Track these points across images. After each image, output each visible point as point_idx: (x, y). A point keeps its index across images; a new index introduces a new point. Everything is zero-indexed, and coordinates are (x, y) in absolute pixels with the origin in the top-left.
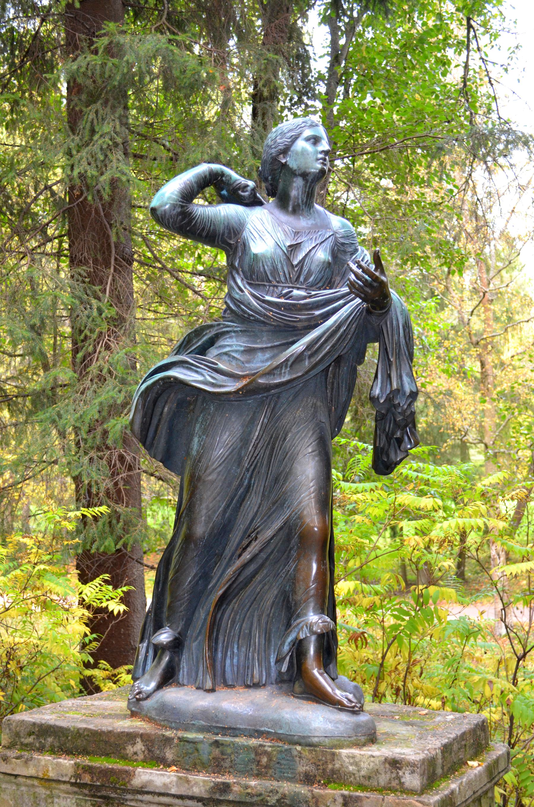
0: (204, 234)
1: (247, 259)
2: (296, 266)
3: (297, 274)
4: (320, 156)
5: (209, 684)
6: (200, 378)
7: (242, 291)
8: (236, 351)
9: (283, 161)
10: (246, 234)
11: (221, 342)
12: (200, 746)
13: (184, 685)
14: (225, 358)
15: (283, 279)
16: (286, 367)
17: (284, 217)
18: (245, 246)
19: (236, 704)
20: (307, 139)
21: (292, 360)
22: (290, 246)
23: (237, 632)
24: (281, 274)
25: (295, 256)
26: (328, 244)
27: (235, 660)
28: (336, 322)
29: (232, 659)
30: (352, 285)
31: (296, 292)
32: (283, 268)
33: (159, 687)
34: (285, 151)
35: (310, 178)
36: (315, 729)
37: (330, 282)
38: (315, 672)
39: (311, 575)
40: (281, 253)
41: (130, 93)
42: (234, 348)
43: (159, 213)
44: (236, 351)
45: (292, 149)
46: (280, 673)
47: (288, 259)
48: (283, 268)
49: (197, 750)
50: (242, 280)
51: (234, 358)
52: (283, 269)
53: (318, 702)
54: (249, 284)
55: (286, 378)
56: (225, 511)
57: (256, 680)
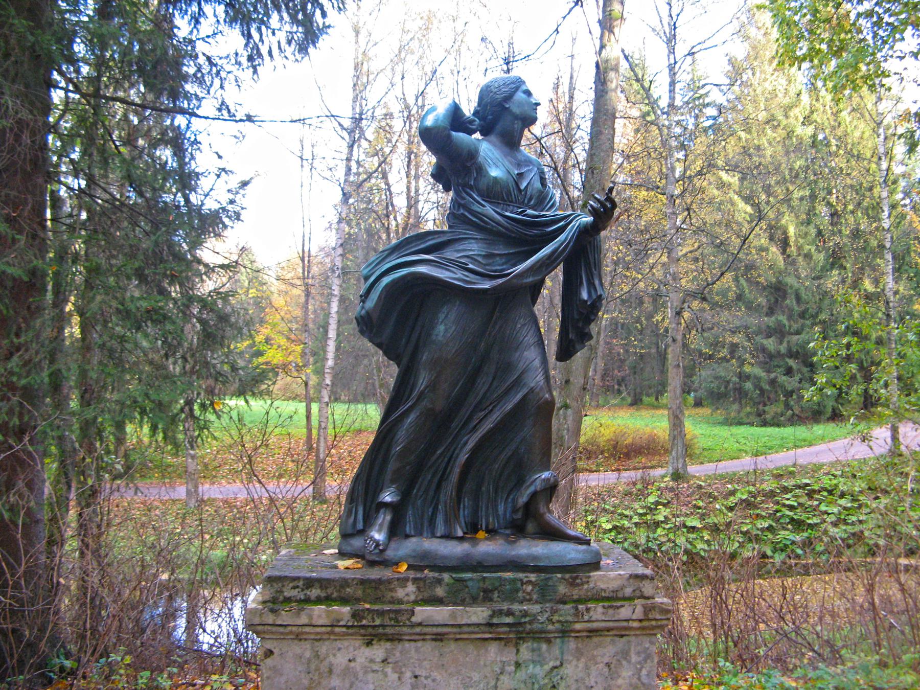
12: (470, 584)
18: (480, 170)
19: (488, 547)
31: (530, 212)
34: (509, 97)
49: (467, 587)
51: (476, 260)
53: (552, 540)
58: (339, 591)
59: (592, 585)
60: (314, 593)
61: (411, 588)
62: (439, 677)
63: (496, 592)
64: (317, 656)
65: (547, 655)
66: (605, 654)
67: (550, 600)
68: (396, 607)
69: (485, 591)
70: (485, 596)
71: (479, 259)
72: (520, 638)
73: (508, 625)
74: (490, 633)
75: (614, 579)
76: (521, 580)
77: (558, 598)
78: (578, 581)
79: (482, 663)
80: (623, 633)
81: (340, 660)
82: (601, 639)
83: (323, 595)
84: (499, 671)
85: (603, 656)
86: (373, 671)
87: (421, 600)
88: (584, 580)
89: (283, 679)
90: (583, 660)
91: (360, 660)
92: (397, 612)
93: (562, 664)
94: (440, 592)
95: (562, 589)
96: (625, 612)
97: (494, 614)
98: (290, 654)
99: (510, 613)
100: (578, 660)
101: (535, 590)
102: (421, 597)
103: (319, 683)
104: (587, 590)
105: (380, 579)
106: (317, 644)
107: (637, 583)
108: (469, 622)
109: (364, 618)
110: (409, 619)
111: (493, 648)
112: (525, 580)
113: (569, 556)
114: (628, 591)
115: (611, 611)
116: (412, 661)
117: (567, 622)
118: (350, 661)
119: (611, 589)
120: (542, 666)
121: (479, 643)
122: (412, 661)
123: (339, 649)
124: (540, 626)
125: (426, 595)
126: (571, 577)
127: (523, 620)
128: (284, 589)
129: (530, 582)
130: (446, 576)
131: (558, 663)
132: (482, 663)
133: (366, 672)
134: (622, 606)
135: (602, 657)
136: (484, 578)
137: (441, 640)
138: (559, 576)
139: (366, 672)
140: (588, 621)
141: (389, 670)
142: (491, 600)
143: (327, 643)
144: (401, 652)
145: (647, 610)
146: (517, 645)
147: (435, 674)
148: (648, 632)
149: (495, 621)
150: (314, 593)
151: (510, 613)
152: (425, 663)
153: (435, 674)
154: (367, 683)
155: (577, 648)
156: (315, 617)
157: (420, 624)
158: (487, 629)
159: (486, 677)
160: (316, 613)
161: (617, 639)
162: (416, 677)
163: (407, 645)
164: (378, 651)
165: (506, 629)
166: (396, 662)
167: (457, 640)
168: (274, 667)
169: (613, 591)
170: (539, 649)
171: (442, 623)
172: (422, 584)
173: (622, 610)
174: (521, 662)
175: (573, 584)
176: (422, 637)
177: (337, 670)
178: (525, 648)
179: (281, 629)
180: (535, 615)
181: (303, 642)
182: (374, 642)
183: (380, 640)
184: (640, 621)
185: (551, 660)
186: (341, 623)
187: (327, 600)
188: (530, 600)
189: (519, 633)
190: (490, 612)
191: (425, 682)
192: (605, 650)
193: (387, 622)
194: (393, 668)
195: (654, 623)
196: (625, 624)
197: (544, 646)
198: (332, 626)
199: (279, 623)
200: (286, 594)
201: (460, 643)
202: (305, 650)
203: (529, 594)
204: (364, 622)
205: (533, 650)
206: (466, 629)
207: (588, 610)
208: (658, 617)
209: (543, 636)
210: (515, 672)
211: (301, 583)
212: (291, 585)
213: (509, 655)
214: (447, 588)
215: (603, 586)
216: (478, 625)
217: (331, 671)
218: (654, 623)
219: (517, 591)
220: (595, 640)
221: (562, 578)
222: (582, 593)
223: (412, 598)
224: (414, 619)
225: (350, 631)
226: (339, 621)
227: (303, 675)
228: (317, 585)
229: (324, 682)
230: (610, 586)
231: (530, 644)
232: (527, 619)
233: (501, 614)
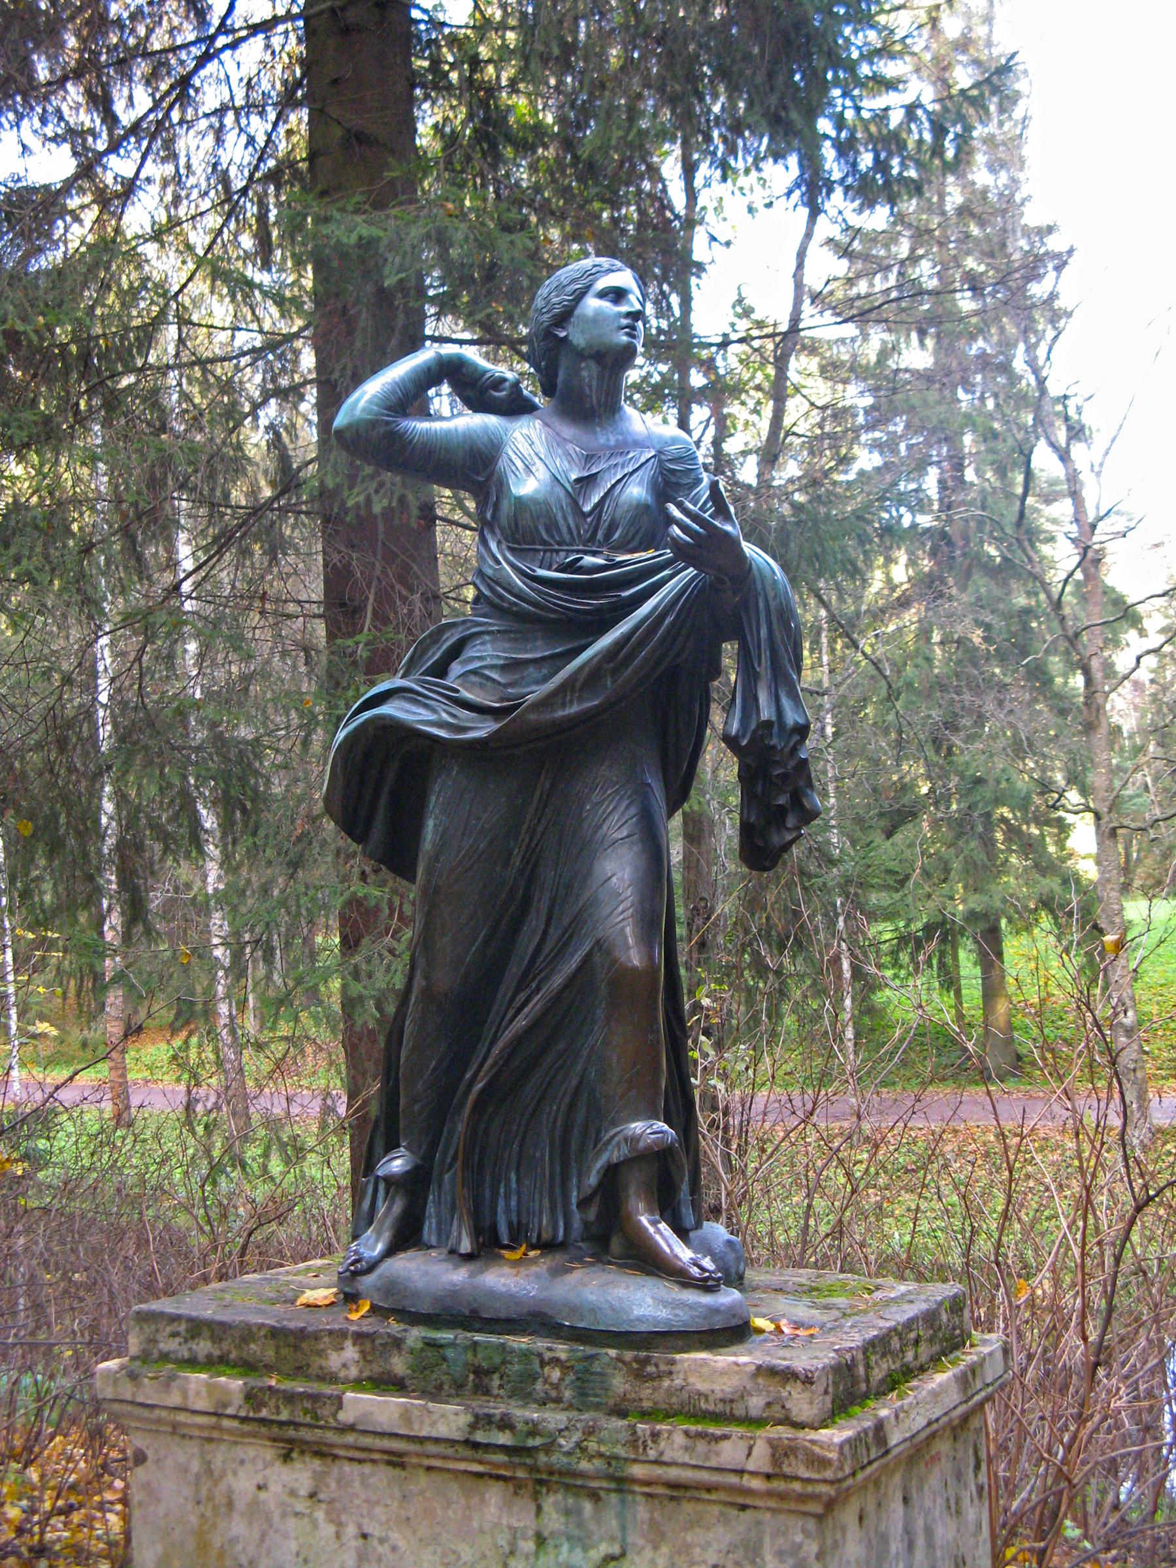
1: (505, 505)
3: (599, 529)
4: (625, 322)
5: (466, 1246)
6: (432, 717)
7: (498, 562)
8: (492, 667)
9: (563, 334)
10: (502, 463)
11: (469, 653)
12: (450, 1353)
13: (430, 1247)
14: (474, 679)
15: (567, 537)
17: (568, 431)
18: (502, 485)
19: (508, 1280)
20: (602, 295)
21: (582, 678)
22: (578, 481)
24: (564, 530)
25: (586, 498)
26: (647, 473)
27: (513, 1203)
28: (655, 608)
29: (507, 1198)
30: (676, 544)
31: (589, 560)
33: (390, 1252)
34: (565, 316)
35: (609, 360)
37: (653, 538)
38: (644, 1220)
40: (562, 494)
42: (488, 662)
43: (347, 435)
44: (492, 667)
45: (578, 312)
46: (586, 1224)
49: (445, 1359)
50: (499, 543)
51: (488, 678)
52: (566, 521)
53: (649, 1273)
54: (511, 549)
56: (487, 942)
57: (545, 1236)
58: (238, 1347)
59: (678, 1382)
60: (203, 1347)
61: (351, 1352)
62: (402, 1544)
63: (496, 1376)
64: (209, 1471)
65: (592, 1526)
66: (709, 1544)
67: (597, 1407)
68: (315, 1387)
69: (478, 1371)
70: (478, 1380)
71: (495, 675)
72: (540, 1482)
73: (504, 1448)
74: (480, 1462)
75: (723, 1373)
76: (540, 1355)
77: (611, 1402)
78: (651, 1369)
79: (475, 1524)
80: (749, 1501)
81: (243, 1484)
82: (700, 1507)
83: (217, 1353)
84: (507, 1549)
85: (705, 1546)
86: (297, 1514)
87: (370, 1379)
88: (663, 1367)
89: (161, 1510)
90: (665, 1549)
91: (275, 1488)
92: (315, 1398)
93: (623, 1554)
94: (399, 1365)
95: (619, 1383)
96: (730, 1452)
97: (481, 1421)
98: (170, 1462)
99: (505, 1424)
100: (656, 1548)
101: (568, 1380)
102: (366, 1374)
103: (215, 1526)
104: (670, 1392)
105: (302, 1330)
106: (208, 1447)
107: (775, 1389)
108: (434, 1434)
109: (264, 1405)
110: (334, 1415)
111: (494, 1494)
112: (548, 1355)
113: (638, 1312)
114: (756, 1404)
115: (701, 1446)
116: (357, 1502)
117: (616, 1458)
118: (259, 1488)
119: (720, 1395)
120: (585, 1550)
121: (469, 1483)
122: (357, 1502)
123: (242, 1462)
124: (565, 1460)
125: (376, 1368)
126: (636, 1359)
127: (531, 1442)
128: (159, 1337)
129: (556, 1361)
130: (415, 1335)
131: (616, 1549)
132: (475, 1524)
133: (284, 1515)
134: (725, 1437)
135: (704, 1549)
136: (475, 1345)
137: (402, 1466)
138: (613, 1352)
139: (284, 1515)
140: (656, 1462)
141: (320, 1515)
142: (487, 1392)
143: (223, 1447)
144: (338, 1482)
145: (780, 1452)
146: (536, 1496)
147: (395, 1536)
148: (793, 1506)
149: (480, 1437)
150: (203, 1347)
151: (505, 1424)
152: (378, 1510)
153: (395, 1536)
154: (286, 1536)
155: (652, 1520)
156: (191, 1394)
157: (352, 1428)
158: (468, 1453)
159: (484, 1557)
160: (192, 1386)
161: (733, 1512)
162: (365, 1536)
163: (347, 1468)
164: (302, 1474)
165: (501, 1458)
166: (331, 1502)
167: (429, 1469)
168: (149, 1484)
169: (723, 1401)
170: (579, 1512)
171: (388, 1429)
172: (368, 1346)
173: (725, 1445)
174: (546, 1534)
175: (639, 1374)
176: (362, 1456)
177: (240, 1504)
178: (550, 1502)
179: (146, 1413)
180: (550, 1435)
181: (187, 1442)
182: (295, 1455)
183: (302, 1452)
184: (768, 1477)
185: (601, 1539)
186: (229, 1411)
187: (212, 1364)
188: (558, 1400)
189: (529, 1470)
190: (469, 1418)
191: (380, 1549)
192: (710, 1535)
193: (300, 1418)
194: (327, 1513)
195: (797, 1486)
196: (733, 1479)
197: (588, 1507)
198: (215, 1414)
199: (140, 1399)
200: (161, 1346)
201: (435, 1476)
202: (187, 1455)
203: (556, 1386)
204: (264, 1413)
205: (567, 1512)
206: (431, 1448)
207: (655, 1436)
208: (804, 1473)
209: (579, 1482)
210: (537, 1554)
211: (182, 1328)
212: (169, 1329)
213: (522, 1518)
214: (410, 1358)
215: (701, 1386)
216: (452, 1442)
217: (230, 1504)
218: (797, 1486)
219: (534, 1378)
220: (688, 1507)
221: (619, 1359)
222: (660, 1396)
223: (354, 1372)
224: (342, 1416)
225: (247, 1428)
226: (225, 1406)
227: (190, 1506)
228: (206, 1333)
229: (222, 1525)
230: (717, 1388)
231: (559, 1497)
232: (537, 1442)
233: (490, 1423)
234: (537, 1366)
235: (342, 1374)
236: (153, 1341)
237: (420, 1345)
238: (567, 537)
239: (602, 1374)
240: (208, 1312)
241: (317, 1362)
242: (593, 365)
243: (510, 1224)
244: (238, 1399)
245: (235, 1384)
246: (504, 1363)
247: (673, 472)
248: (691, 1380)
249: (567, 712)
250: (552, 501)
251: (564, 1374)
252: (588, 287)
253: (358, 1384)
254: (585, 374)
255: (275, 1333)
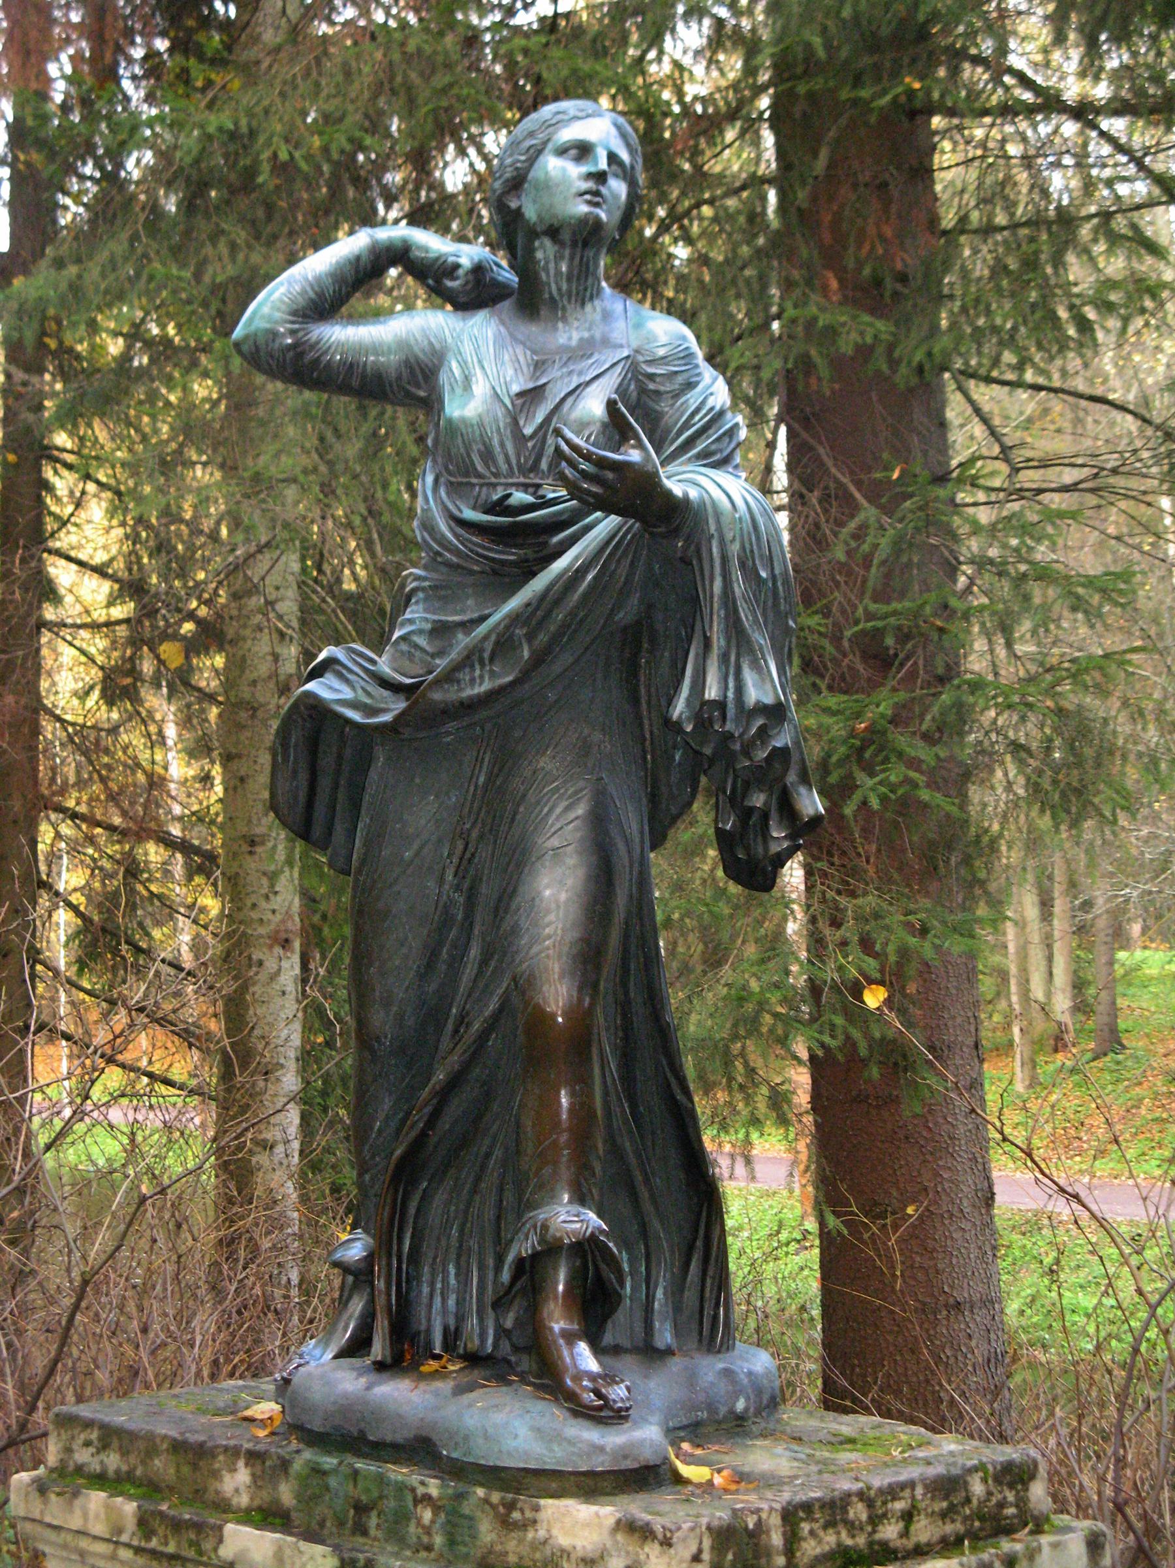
0: (355, 383)
2: (532, 437)
10: (443, 378)
12: (333, 1482)
15: (504, 467)
16: (482, 664)
19: (404, 1398)
20: (562, 152)
21: (489, 646)
22: (520, 395)
23: (454, 1242)
24: (501, 459)
27: (451, 1302)
32: (502, 445)
36: (509, 1454)
39: (558, 1113)
40: (500, 412)
41: (1103, 37)
47: (515, 422)
48: (502, 445)
52: (505, 449)
55: (486, 686)
58: (143, 1462)
59: (542, 1533)
63: (374, 1513)
78: (516, 1515)
83: (124, 1468)
102: (257, 1503)
105: (202, 1445)
110: (216, 1550)
112: (421, 1490)
113: (510, 1444)
119: (580, 1554)
129: (427, 1498)
138: (480, 1492)
142: (365, 1533)
150: (113, 1461)
188: (429, 1548)
199: (48, 1519)
203: (428, 1531)
204: (154, 1543)
211: (94, 1435)
221: (486, 1501)
223: (244, 1500)
234: (410, 1504)
235: (235, 1501)
236: (69, 1450)
237: (306, 1471)
238: (504, 467)
239: (471, 1519)
240: (120, 1420)
241: (214, 1485)
242: (547, 242)
243: (446, 1330)
244: (130, 1524)
245: (129, 1508)
246: (381, 1497)
247: (651, 377)
248: (555, 1532)
249: (476, 691)
250: (486, 421)
251: (435, 1513)
252: (545, 143)
253: (247, 1517)
254: (539, 255)
255: (178, 1447)
